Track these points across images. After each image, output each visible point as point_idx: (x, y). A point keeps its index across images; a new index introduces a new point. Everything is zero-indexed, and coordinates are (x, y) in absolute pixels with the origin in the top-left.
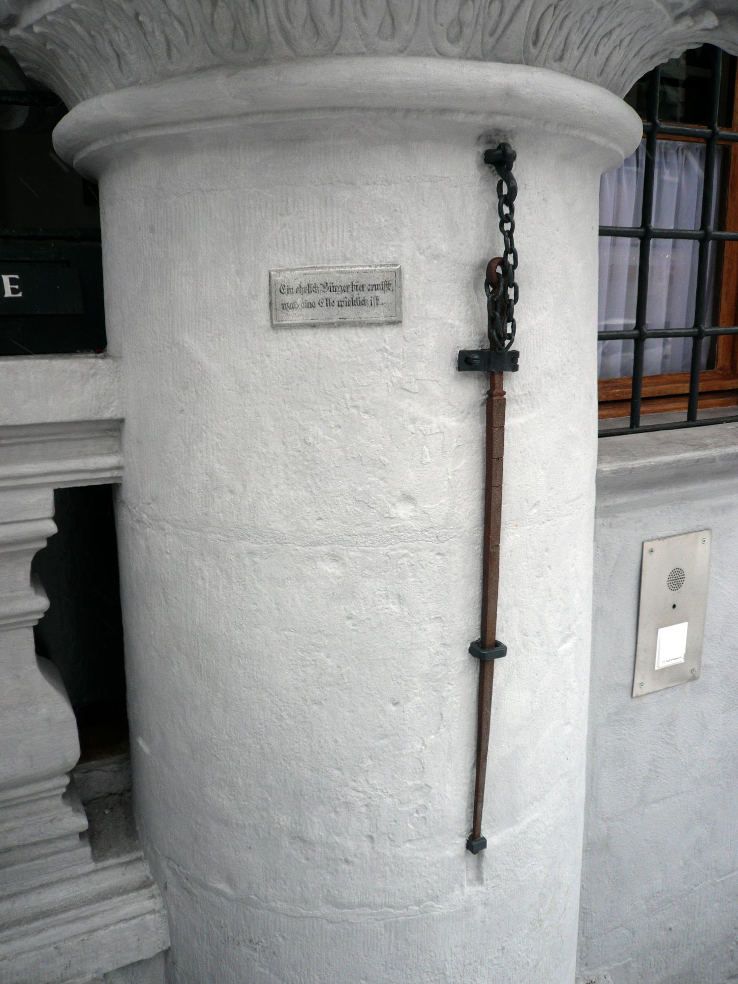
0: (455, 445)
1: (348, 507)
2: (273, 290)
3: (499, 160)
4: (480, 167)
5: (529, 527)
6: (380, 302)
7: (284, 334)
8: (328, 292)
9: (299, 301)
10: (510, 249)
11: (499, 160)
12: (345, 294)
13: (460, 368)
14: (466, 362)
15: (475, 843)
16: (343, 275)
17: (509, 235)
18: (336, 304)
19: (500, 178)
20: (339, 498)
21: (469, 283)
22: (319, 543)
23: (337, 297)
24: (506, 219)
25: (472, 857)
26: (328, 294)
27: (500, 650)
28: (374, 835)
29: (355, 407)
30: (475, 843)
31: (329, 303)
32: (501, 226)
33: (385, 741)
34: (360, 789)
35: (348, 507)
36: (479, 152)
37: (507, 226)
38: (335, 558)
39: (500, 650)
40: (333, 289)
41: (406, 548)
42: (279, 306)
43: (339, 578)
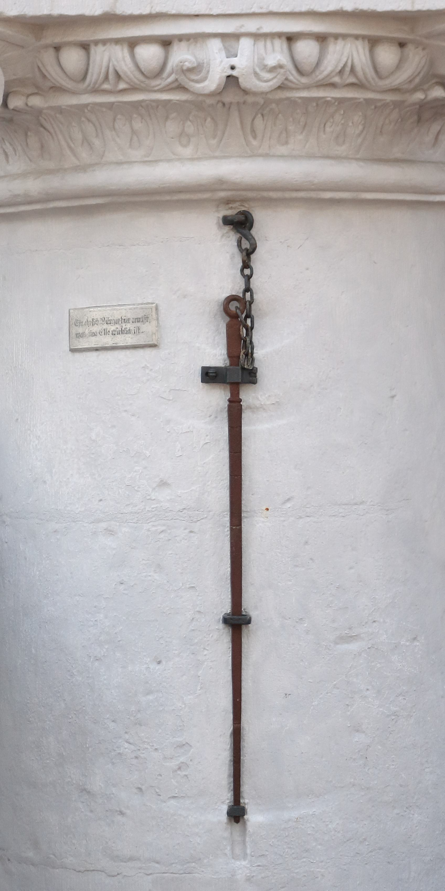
0: (202, 443)
1: (120, 490)
2: (71, 323)
3: (241, 224)
4: (219, 227)
5: (282, 519)
6: (141, 331)
7: (77, 355)
8: (105, 324)
9: (87, 332)
10: (248, 289)
11: (241, 224)
12: (117, 326)
13: (203, 381)
14: (210, 376)
15: (237, 814)
16: (115, 312)
17: (248, 278)
18: (111, 332)
19: (239, 235)
20: (114, 484)
21: (216, 315)
22: (99, 521)
23: (112, 328)
24: (246, 265)
25: (237, 827)
26: (105, 326)
27: (226, 621)
28: (143, 788)
29: (126, 411)
30: (237, 814)
31: (106, 332)
32: (242, 271)
33: (151, 697)
34: (131, 741)
35: (120, 490)
36: (219, 217)
37: (247, 272)
38: (110, 532)
39: (226, 621)
40: (109, 322)
41: (164, 525)
42: (74, 335)
43: (114, 549)
